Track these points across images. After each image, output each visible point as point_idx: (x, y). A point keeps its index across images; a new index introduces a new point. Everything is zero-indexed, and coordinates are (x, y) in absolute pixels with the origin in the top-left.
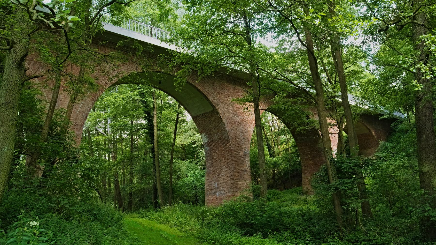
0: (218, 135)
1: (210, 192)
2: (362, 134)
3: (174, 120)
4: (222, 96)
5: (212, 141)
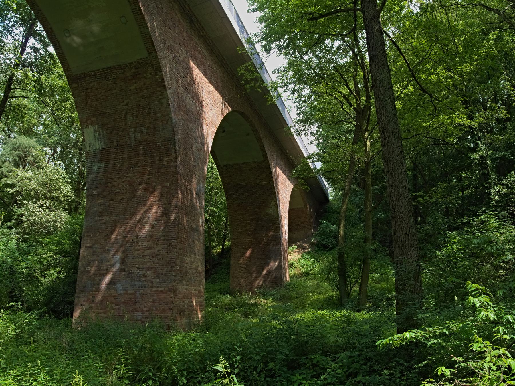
0: (141, 132)
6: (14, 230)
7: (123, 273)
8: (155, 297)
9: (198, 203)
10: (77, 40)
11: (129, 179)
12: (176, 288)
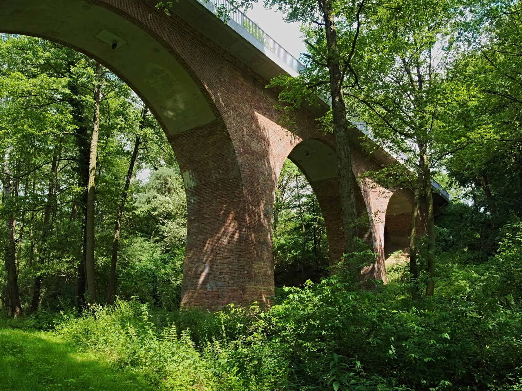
0: (219, 173)
1: (192, 281)
2: (403, 214)
3: (129, 153)
5: (205, 185)
6: (159, 245)
7: (211, 277)
8: (230, 294)
9: (266, 222)
10: (171, 113)
11: (213, 207)
12: (245, 288)
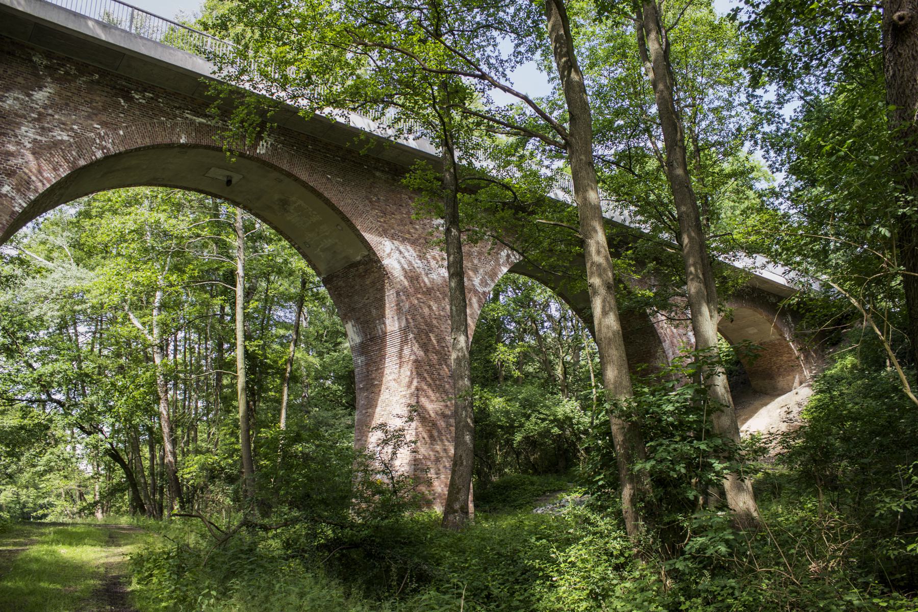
4: (393, 221)
